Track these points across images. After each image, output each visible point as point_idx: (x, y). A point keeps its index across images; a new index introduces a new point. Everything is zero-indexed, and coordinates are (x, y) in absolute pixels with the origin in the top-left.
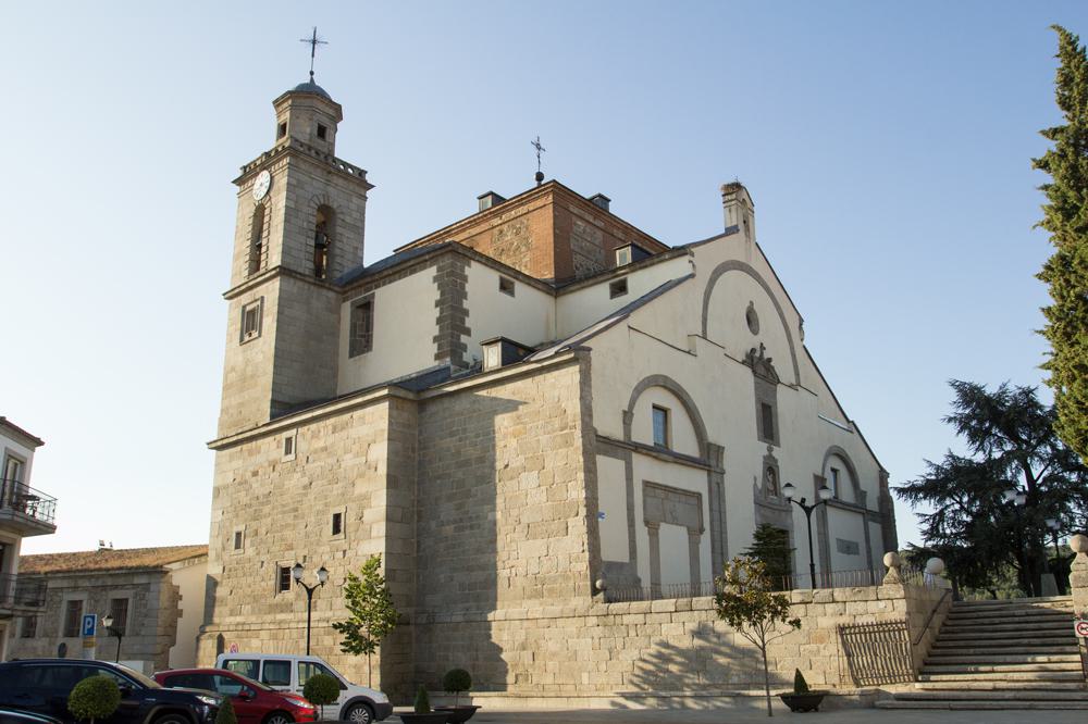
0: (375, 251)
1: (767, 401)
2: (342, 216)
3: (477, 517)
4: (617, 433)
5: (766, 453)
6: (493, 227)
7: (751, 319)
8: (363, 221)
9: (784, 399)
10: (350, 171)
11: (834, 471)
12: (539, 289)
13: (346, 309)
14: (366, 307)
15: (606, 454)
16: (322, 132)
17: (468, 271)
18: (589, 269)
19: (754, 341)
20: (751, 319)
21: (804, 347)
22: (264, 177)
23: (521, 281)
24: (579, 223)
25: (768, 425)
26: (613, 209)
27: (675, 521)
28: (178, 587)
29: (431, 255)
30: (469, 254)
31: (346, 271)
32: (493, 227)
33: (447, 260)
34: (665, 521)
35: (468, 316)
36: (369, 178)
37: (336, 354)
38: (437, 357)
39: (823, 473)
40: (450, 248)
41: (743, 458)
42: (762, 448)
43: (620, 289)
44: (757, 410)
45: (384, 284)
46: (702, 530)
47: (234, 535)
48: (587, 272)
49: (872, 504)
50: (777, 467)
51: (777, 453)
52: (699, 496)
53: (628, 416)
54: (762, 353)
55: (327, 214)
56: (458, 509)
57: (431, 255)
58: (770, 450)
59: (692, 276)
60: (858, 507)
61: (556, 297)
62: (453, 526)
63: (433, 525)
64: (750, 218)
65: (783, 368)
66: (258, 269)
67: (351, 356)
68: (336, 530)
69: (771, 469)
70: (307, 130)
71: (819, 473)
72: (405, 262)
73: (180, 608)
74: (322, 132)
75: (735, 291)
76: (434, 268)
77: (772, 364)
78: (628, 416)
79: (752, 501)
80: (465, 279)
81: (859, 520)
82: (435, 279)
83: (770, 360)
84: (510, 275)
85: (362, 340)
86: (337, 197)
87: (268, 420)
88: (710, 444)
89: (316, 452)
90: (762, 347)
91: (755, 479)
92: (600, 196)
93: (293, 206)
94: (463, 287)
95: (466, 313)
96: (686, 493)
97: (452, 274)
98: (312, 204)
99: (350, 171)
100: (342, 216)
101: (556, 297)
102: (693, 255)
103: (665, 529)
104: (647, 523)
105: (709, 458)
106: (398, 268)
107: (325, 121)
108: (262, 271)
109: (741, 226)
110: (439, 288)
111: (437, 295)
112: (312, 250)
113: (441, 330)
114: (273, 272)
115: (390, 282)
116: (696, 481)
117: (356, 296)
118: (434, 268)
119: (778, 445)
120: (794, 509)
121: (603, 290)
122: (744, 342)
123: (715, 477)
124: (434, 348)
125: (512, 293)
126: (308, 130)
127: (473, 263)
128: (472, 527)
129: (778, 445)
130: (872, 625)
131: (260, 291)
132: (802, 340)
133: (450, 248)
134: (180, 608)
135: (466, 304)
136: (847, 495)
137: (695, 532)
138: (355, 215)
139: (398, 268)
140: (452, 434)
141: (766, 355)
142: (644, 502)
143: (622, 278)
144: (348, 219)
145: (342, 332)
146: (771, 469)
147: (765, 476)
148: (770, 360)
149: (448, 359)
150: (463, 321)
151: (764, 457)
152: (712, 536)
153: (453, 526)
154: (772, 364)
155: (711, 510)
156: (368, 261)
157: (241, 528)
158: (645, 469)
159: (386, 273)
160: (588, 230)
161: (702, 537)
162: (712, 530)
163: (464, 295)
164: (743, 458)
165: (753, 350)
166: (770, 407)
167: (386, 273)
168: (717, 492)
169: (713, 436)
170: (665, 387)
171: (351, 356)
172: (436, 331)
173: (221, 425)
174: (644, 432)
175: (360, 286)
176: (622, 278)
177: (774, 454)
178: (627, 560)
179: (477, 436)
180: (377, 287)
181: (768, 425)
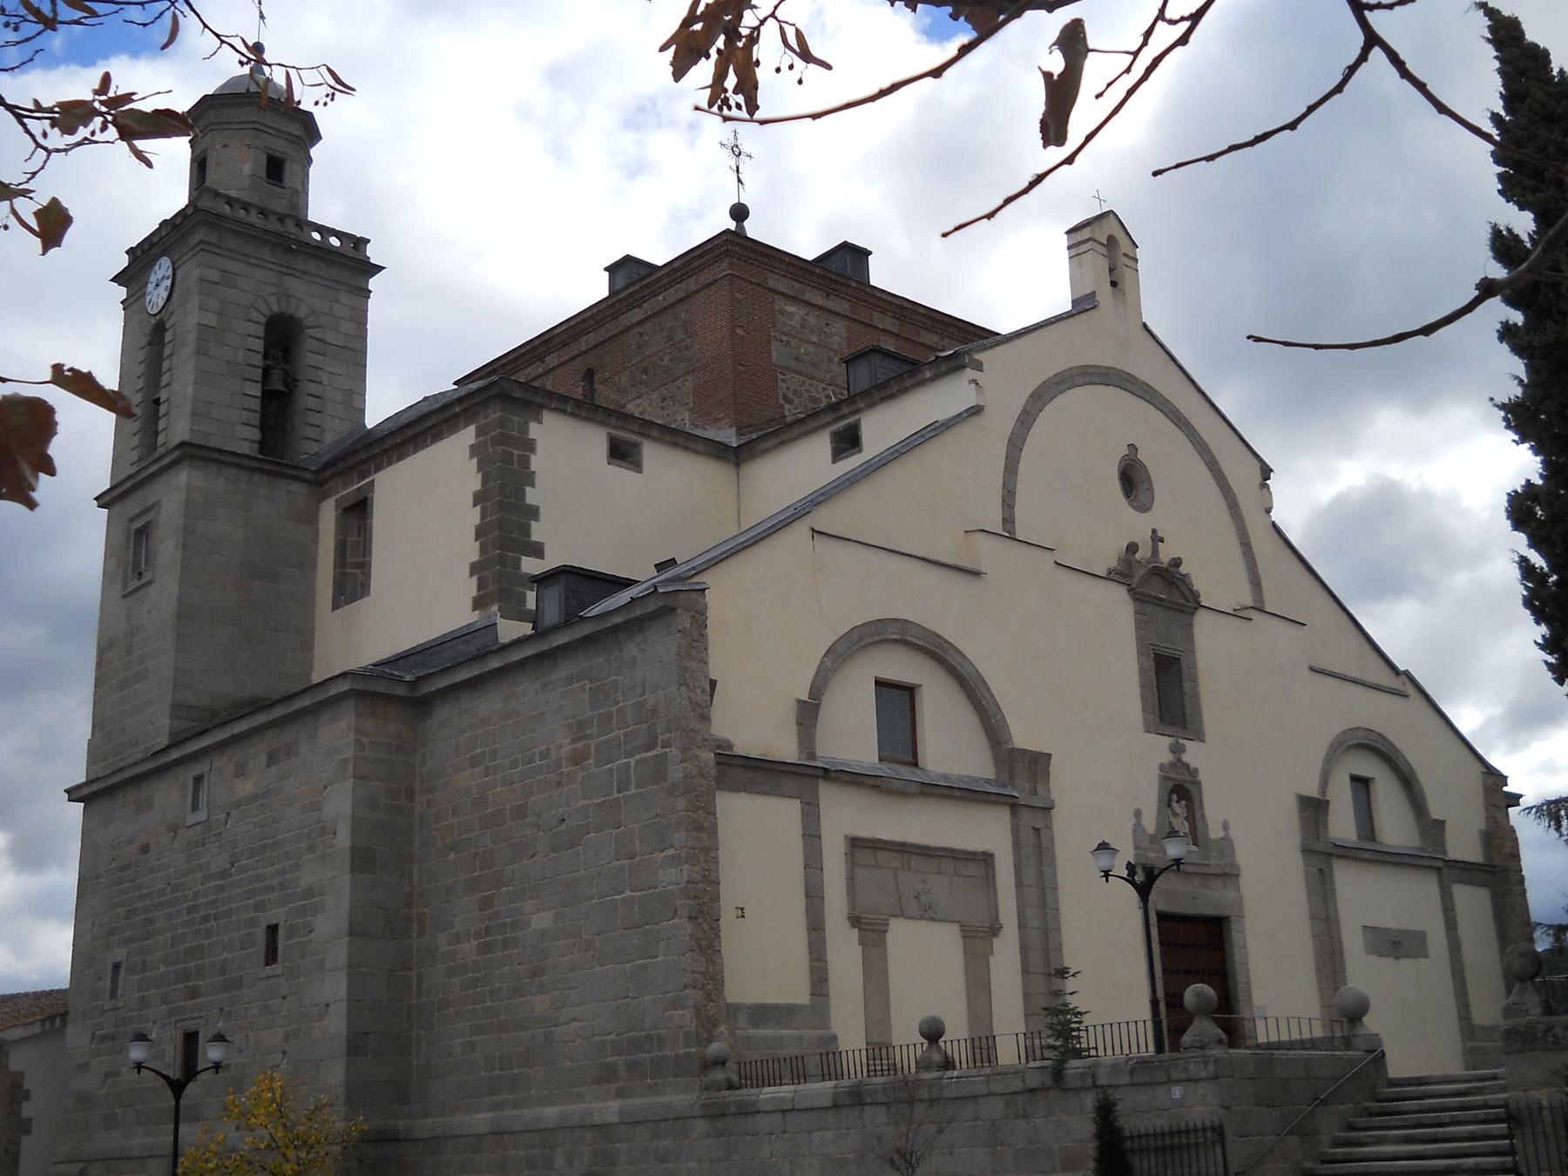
0: (385, 397)
1: (1168, 648)
2: (317, 333)
3: (514, 925)
4: (786, 749)
5: (1167, 758)
6: (628, 329)
7: (1132, 479)
8: (362, 336)
9: (1214, 646)
10: (335, 242)
11: (1361, 784)
12: (697, 452)
13: (328, 513)
14: (358, 510)
15: (735, 788)
16: (275, 169)
17: (534, 430)
18: (813, 400)
19: (1138, 526)
20: (1132, 479)
21: (1274, 525)
22: (163, 267)
23: (656, 440)
24: (791, 309)
25: (1170, 693)
26: (881, 276)
27: (929, 913)
28: (21, 1074)
29: (465, 405)
30: (538, 400)
31: (329, 438)
32: (628, 329)
33: (494, 414)
34: (903, 915)
35: (537, 520)
36: (373, 254)
37: (309, 600)
38: (478, 604)
39: (1323, 791)
40: (494, 391)
41: (1105, 785)
42: (1158, 748)
43: (848, 442)
44: (1142, 670)
45: (390, 463)
46: (995, 930)
47: (110, 968)
48: (810, 405)
49: (1464, 845)
50: (1198, 784)
51: (1194, 754)
52: (986, 859)
53: (808, 713)
54: (1155, 551)
55: (282, 337)
56: (482, 909)
57: (465, 405)
58: (1177, 750)
59: (976, 411)
60: (1429, 858)
61: (737, 465)
62: (474, 943)
63: (443, 939)
64: (1128, 273)
65: (1215, 577)
66: (154, 448)
67: (336, 605)
68: (271, 956)
69: (1180, 790)
70: (240, 169)
71: (1313, 791)
72: (422, 426)
73: (25, 1114)
74: (275, 169)
75: (1092, 428)
76: (472, 429)
77: (1183, 569)
78: (808, 713)
79: (1298, 849)
80: (530, 446)
81: (1428, 886)
82: (474, 450)
83: (1177, 562)
84: (628, 430)
85: (352, 583)
86: (307, 298)
87: (163, 741)
88: (1014, 752)
89: (238, 804)
90: (1156, 539)
91: (1138, 814)
92: (846, 246)
93: (214, 324)
94: (525, 463)
95: (533, 513)
96: (971, 857)
97: (502, 440)
98: (254, 315)
99: (335, 242)
100: (317, 333)
101: (737, 465)
102: (979, 366)
103: (902, 935)
104: (855, 921)
105: (1019, 782)
106: (411, 432)
107: (280, 147)
108: (161, 451)
109: (1105, 293)
110: (480, 468)
111: (474, 483)
112: (256, 404)
113: (483, 550)
114: (176, 454)
115: (399, 459)
116: (987, 832)
117: (345, 486)
118: (472, 429)
119: (1199, 736)
120: (1522, 835)
121: (818, 447)
122: (1114, 527)
123: (1026, 818)
124: (470, 587)
125: (637, 466)
126: (247, 169)
127: (547, 416)
128: (505, 944)
129: (1199, 736)
130: (1204, 1130)
131: (155, 492)
132: (1268, 511)
133: (494, 391)
134: (25, 1114)
135: (532, 496)
136: (1396, 828)
137: (979, 938)
138: (345, 327)
139: (411, 432)
140: (473, 763)
141: (1166, 555)
142: (851, 880)
143: (851, 420)
144: (331, 338)
145: (320, 558)
146: (1180, 790)
147: (1166, 803)
148: (1177, 562)
149: (495, 608)
150: (526, 531)
151: (1162, 767)
152: (1024, 950)
153: (474, 943)
154: (1183, 569)
155: (1019, 885)
156: (374, 417)
157: (120, 954)
158: (846, 815)
159: (390, 442)
160: (812, 320)
161: (997, 943)
162: (1022, 926)
163: (530, 480)
164: (1105, 785)
165: (1132, 548)
166: (1176, 660)
167: (390, 442)
168: (1036, 850)
169: (1022, 737)
170: (904, 643)
171: (336, 605)
172: (473, 552)
173: (92, 761)
174: (852, 734)
175: (350, 469)
176: (851, 420)
177: (1186, 758)
178: (803, 998)
179: (514, 765)
180: (378, 468)
181: (1170, 693)
